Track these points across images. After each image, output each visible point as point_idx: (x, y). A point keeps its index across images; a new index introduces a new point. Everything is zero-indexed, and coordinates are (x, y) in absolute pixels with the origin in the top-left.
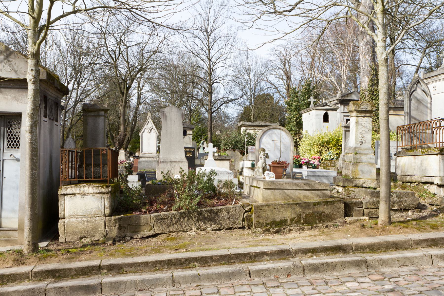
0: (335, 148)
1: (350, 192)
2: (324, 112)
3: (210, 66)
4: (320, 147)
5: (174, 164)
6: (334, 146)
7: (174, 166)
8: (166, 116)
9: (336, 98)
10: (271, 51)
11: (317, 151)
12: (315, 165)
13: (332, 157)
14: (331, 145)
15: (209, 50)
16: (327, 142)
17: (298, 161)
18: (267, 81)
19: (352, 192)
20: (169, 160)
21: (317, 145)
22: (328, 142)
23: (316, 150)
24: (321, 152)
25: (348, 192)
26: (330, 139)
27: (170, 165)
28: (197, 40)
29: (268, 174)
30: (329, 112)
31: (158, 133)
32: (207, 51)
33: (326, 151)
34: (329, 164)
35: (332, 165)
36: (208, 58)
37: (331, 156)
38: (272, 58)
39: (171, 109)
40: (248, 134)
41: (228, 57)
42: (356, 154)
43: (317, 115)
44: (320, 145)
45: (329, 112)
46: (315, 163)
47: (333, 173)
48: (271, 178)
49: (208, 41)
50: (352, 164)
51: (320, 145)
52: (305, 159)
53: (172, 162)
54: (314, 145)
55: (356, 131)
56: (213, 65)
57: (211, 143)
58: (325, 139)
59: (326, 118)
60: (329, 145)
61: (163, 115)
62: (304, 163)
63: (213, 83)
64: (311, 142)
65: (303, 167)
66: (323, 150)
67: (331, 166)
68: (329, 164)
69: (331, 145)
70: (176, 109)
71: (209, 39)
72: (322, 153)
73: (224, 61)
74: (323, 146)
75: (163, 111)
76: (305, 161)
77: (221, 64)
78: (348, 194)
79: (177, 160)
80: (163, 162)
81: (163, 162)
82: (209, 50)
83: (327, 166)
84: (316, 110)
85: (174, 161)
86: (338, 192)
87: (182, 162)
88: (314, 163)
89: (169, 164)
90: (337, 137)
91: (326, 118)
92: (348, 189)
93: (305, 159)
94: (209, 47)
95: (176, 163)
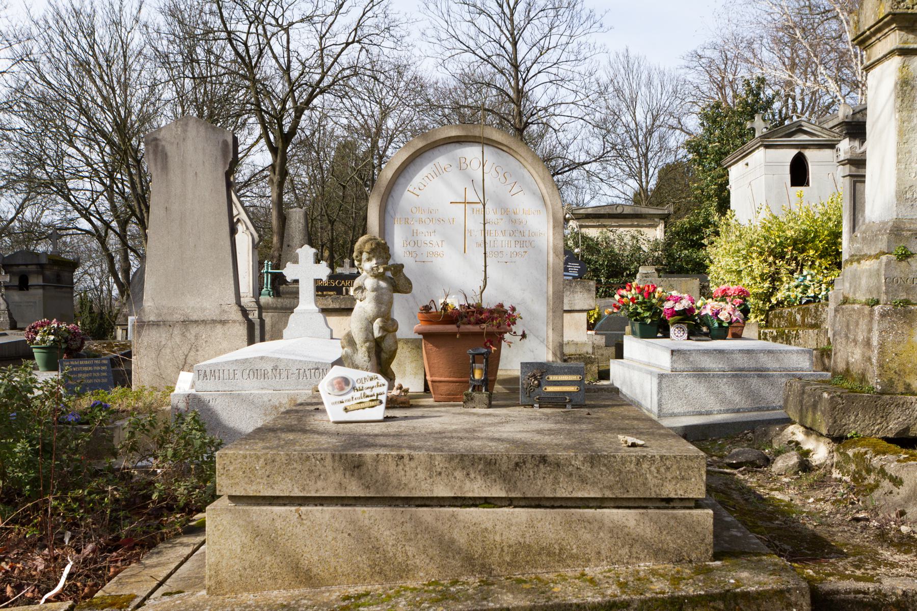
0: (825, 263)
1: (871, 479)
2: (794, 152)
3: (518, 84)
4: (771, 259)
5: (194, 330)
6: (821, 257)
7: (197, 337)
8: (165, 156)
9: (836, 122)
10: (689, 59)
11: (762, 276)
12: (721, 322)
13: (810, 293)
14: (812, 252)
15: (515, 44)
16: (795, 242)
17: (650, 308)
18: (682, 130)
19: (886, 484)
20: (177, 317)
21: (761, 254)
22: (801, 243)
23: (757, 273)
24: (774, 278)
25: (857, 478)
26: (806, 232)
27: (183, 335)
28: (482, 21)
29: (346, 381)
30: (808, 153)
31: (256, 235)
32: (508, 46)
33: (792, 272)
34: (798, 317)
35: (809, 320)
36: (512, 64)
37: (807, 288)
38: (692, 76)
39: (185, 131)
40: (585, 238)
41: (563, 58)
42: (905, 256)
43: (768, 165)
44: (772, 252)
45: (809, 154)
46: (723, 316)
47: (797, 357)
48: (361, 406)
49: (512, 21)
50: (883, 315)
51: (772, 252)
52: (678, 300)
53: (187, 323)
54: (749, 253)
55: (901, 133)
56: (524, 84)
57: (306, 247)
58: (789, 233)
59: (799, 173)
60: (803, 251)
61: (155, 152)
62: (674, 313)
63: (527, 124)
64: (740, 245)
65: (673, 330)
66: (783, 271)
67: (804, 325)
68: (798, 317)
69: (812, 252)
70: (202, 130)
71: (512, 15)
72: (780, 280)
73: (553, 70)
74: (783, 258)
75: (156, 139)
76: (678, 307)
77: (542, 77)
78: (860, 487)
79: (210, 314)
80: (156, 324)
81: (156, 324)
82: (515, 44)
83: (793, 324)
84: (767, 147)
85: (195, 318)
86: (805, 466)
87: (223, 322)
88: (716, 314)
89: (177, 331)
90: (831, 224)
91: (799, 173)
92: (860, 457)
93: (678, 300)
94: (512, 34)
95: (201, 327)
